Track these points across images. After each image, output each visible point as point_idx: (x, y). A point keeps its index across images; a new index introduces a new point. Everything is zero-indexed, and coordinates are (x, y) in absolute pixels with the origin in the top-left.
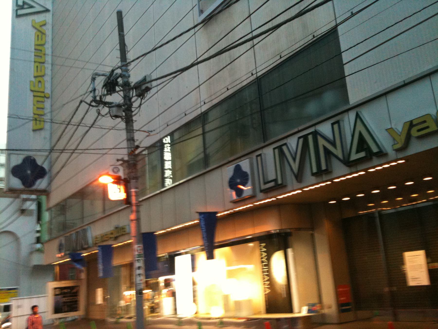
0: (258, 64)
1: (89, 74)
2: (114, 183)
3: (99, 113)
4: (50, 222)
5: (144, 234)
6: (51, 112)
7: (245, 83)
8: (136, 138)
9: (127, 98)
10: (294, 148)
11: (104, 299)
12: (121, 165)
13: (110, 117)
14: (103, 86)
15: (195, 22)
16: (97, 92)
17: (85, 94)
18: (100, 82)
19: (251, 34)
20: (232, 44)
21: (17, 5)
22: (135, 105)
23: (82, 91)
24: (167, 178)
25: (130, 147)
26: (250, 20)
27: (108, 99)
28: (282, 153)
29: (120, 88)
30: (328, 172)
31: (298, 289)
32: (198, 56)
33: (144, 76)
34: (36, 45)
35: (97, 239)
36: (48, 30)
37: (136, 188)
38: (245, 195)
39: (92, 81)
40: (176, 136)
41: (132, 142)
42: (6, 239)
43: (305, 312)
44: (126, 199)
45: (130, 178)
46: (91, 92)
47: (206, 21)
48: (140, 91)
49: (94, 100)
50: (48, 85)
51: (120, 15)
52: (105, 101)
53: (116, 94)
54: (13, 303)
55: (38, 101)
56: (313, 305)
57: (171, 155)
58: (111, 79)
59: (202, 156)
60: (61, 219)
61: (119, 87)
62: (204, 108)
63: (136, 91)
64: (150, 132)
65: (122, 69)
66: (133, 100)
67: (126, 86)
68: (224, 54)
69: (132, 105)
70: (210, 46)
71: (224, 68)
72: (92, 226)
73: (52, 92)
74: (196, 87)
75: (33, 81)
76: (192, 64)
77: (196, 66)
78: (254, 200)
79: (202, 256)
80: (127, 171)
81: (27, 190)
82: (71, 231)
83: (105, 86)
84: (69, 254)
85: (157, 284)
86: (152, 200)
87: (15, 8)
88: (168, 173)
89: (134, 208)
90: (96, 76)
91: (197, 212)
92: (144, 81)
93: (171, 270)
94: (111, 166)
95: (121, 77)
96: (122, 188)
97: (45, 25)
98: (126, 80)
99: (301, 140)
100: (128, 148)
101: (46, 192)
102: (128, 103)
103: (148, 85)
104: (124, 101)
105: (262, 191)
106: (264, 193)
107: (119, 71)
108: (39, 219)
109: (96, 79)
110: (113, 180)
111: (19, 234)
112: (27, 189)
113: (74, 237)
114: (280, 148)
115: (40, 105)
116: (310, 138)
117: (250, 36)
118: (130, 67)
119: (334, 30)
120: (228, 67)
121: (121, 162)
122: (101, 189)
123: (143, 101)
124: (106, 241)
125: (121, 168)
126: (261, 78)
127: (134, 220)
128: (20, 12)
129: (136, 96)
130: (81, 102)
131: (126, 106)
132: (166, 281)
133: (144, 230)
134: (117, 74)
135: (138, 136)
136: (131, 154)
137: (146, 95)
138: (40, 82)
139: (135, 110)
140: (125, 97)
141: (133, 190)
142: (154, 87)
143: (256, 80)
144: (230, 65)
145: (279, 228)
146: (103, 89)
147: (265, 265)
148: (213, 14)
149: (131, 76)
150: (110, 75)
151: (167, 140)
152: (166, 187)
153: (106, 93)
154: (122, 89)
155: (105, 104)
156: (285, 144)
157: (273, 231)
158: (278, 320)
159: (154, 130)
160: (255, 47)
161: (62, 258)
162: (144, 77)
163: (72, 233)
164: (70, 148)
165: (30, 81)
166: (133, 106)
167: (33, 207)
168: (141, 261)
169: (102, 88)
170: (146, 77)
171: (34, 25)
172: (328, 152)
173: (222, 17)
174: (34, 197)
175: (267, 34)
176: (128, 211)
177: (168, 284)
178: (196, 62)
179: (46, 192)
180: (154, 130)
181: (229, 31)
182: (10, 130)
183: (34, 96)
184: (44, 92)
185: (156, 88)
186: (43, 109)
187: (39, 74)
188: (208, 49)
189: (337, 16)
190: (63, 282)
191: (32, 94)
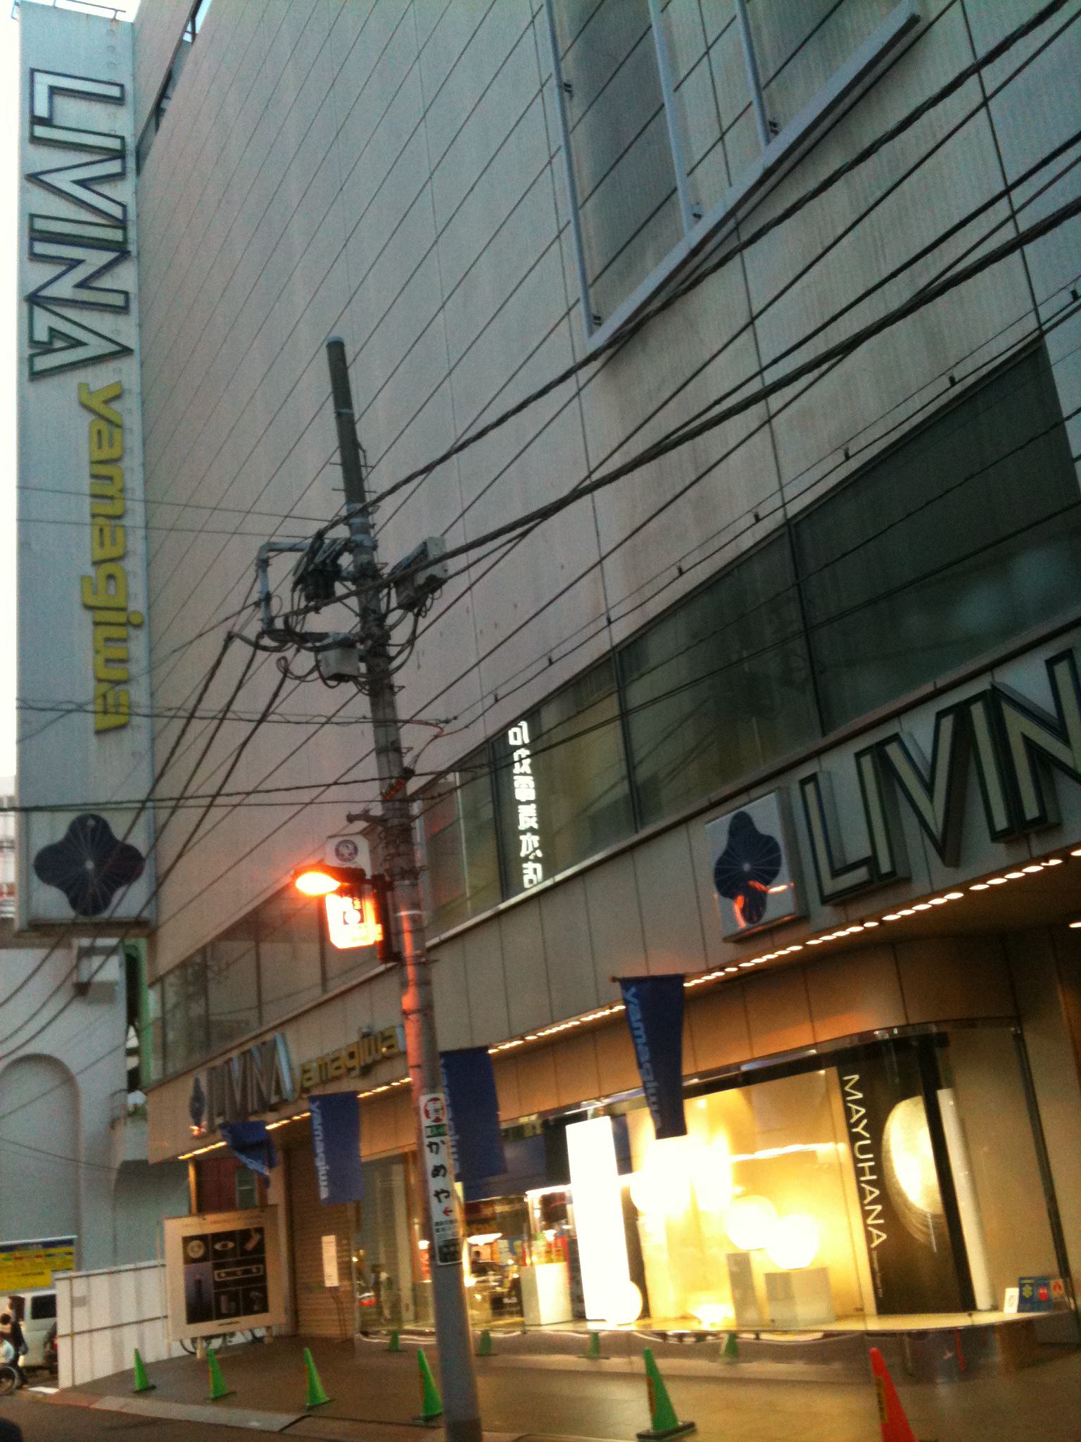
0: (788, 475)
1: (243, 554)
2: (341, 892)
3: (286, 672)
4: (163, 1022)
5: (452, 1058)
6: (151, 669)
7: (747, 542)
8: (405, 744)
9: (372, 617)
10: (928, 751)
11: (345, 1269)
12: (364, 833)
13: (320, 681)
14: (296, 584)
15: (577, 350)
16: (275, 603)
17: (239, 613)
18: (284, 567)
19: (758, 378)
20: (717, 402)
21: (33, 342)
22: (399, 636)
23: (235, 603)
24: (526, 859)
25: (386, 775)
26: (752, 335)
27: (316, 623)
28: (886, 770)
29: (348, 588)
30: (1047, 825)
31: (981, 1224)
32: (593, 465)
33: (420, 542)
34: (92, 463)
35: (307, 1076)
36: (130, 412)
37: (415, 905)
38: (772, 912)
39: (260, 572)
40: (549, 717)
41: (392, 756)
42: (34, 1082)
43: (1010, 1310)
44: (381, 943)
45: (392, 876)
46: (257, 604)
47: (626, 339)
48: (412, 594)
49: (269, 630)
50: (137, 587)
51: (336, 350)
52: (303, 631)
53: (338, 605)
54: (62, 1292)
55: (108, 640)
56: (1042, 1281)
57: (532, 784)
58: (318, 559)
59: (624, 788)
60: (197, 1009)
61: (346, 583)
62: (621, 632)
63: (397, 592)
64: (442, 725)
65: (350, 526)
66: (391, 619)
67: (367, 576)
68: (673, 454)
69: (389, 637)
70: (631, 429)
71: (677, 497)
72: (290, 1033)
73: (149, 608)
74: (591, 564)
75: (90, 577)
76: (575, 490)
77: (588, 498)
78: (803, 930)
79: (644, 1125)
80: (381, 851)
81: (85, 924)
82: (247, 1041)
83: (302, 580)
84: (222, 1127)
85: (523, 1214)
86: (471, 943)
87: (29, 352)
88: (529, 843)
89: (411, 971)
90: (271, 554)
91: (614, 979)
92: (421, 558)
93: (557, 1168)
94: (330, 837)
95: (351, 551)
96: (369, 907)
97: (117, 397)
98: (364, 558)
99: (947, 723)
100: (381, 779)
101: (144, 926)
102: (375, 630)
103: (435, 570)
104: (362, 628)
105: (825, 900)
106: (836, 905)
107: (342, 532)
108: (133, 1013)
109: (271, 561)
110: (336, 884)
111: (73, 1062)
112: (82, 919)
113: (236, 1068)
114: (878, 752)
115: (116, 652)
116: (978, 711)
117: (755, 387)
118: (378, 517)
119: (1035, 347)
120: (690, 492)
121: (362, 825)
122: (314, 906)
123: (423, 623)
124: (337, 1078)
125: (363, 845)
126: (797, 523)
127: (413, 1012)
128: (43, 363)
129: (399, 607)
130: (230, 638)
131: (370, 643)
132: (547, 1201)
133: (447, 1042)
134: (334, 541)
135: (410, 737)
136: (394, 792)
137: (428, 602)
138: (111, 577)
139: (399, 653)
140: (364, 614)
141: (404, 913)
142: (451, 577)
143: (785, 529)
144: (695, 487)
145: (902, 1022)
146: (297, 594)
147: (863, 1150)
148: (646, 312)
149: (381, 545)
150: (312, 545)
151: (520, 735)
152: (526, 889)
153: (303, 604)
154: (353, 588)
155: (304, 640)
156: (895, 738)
157: (877, 1033)
158: (922, 1334)
159: (455, 718)
160: (775, 421)
161: (202, 1140)
162: (420, 546)
163: (229, 1056)
164: (200, 793)
165: (83, 578)
166: (390, 642)
167: (112, 971)
168: (443, 1148)
169: (294, 590)
170: (428, 544)
171: (87, 402)
172: (1041, 760)
173: (662, 332)
174: (111, 942)
175: (816, 373)
176: (393, 982)
177: (555, 1211)
178: (588, 482)
179: (144, 926)
180: (455, 718)
181: (688, 375)
182: (26, 738)
183: (96, 624)
184: (123, 609)
185: (464, 576)
186: (122, 661)
187: (109, 552)
188: (622, 439)
189: (1038, 301)
190: (211, 1218)
191: (88, 617)
